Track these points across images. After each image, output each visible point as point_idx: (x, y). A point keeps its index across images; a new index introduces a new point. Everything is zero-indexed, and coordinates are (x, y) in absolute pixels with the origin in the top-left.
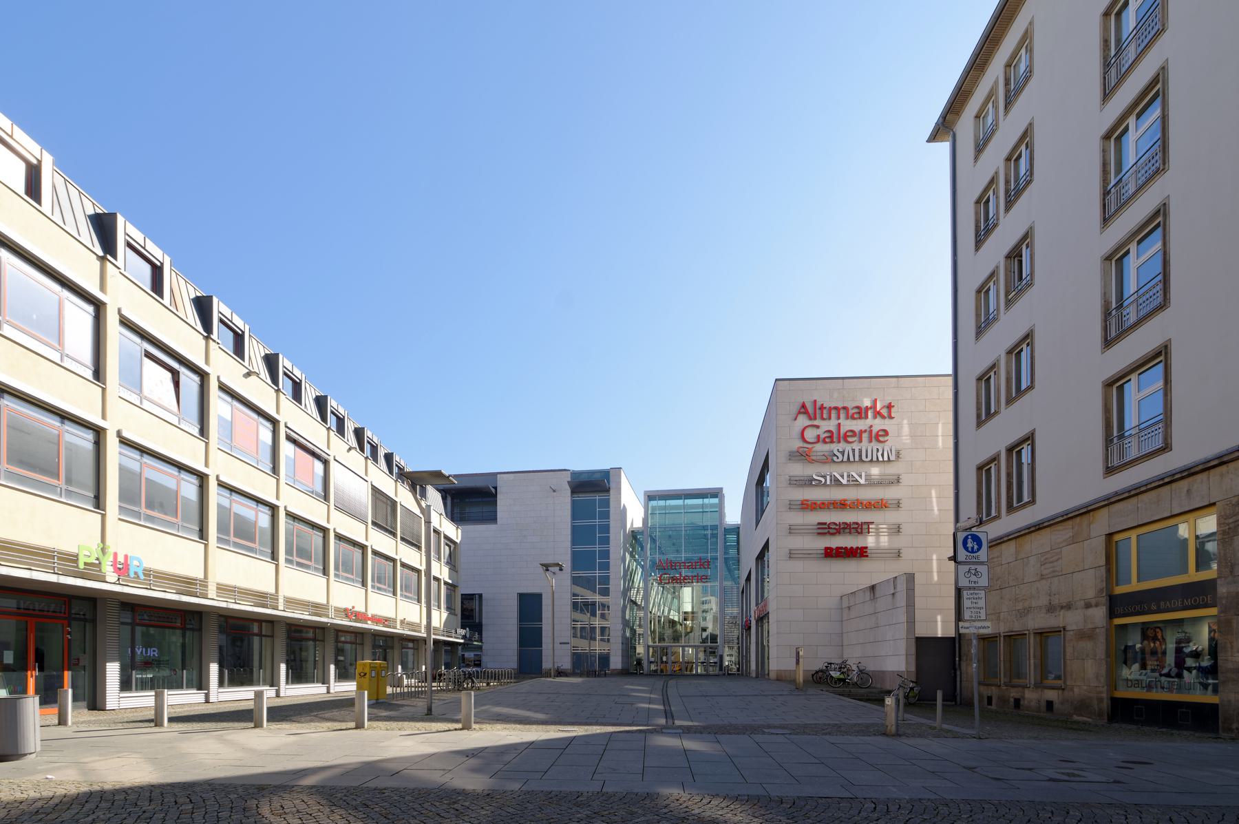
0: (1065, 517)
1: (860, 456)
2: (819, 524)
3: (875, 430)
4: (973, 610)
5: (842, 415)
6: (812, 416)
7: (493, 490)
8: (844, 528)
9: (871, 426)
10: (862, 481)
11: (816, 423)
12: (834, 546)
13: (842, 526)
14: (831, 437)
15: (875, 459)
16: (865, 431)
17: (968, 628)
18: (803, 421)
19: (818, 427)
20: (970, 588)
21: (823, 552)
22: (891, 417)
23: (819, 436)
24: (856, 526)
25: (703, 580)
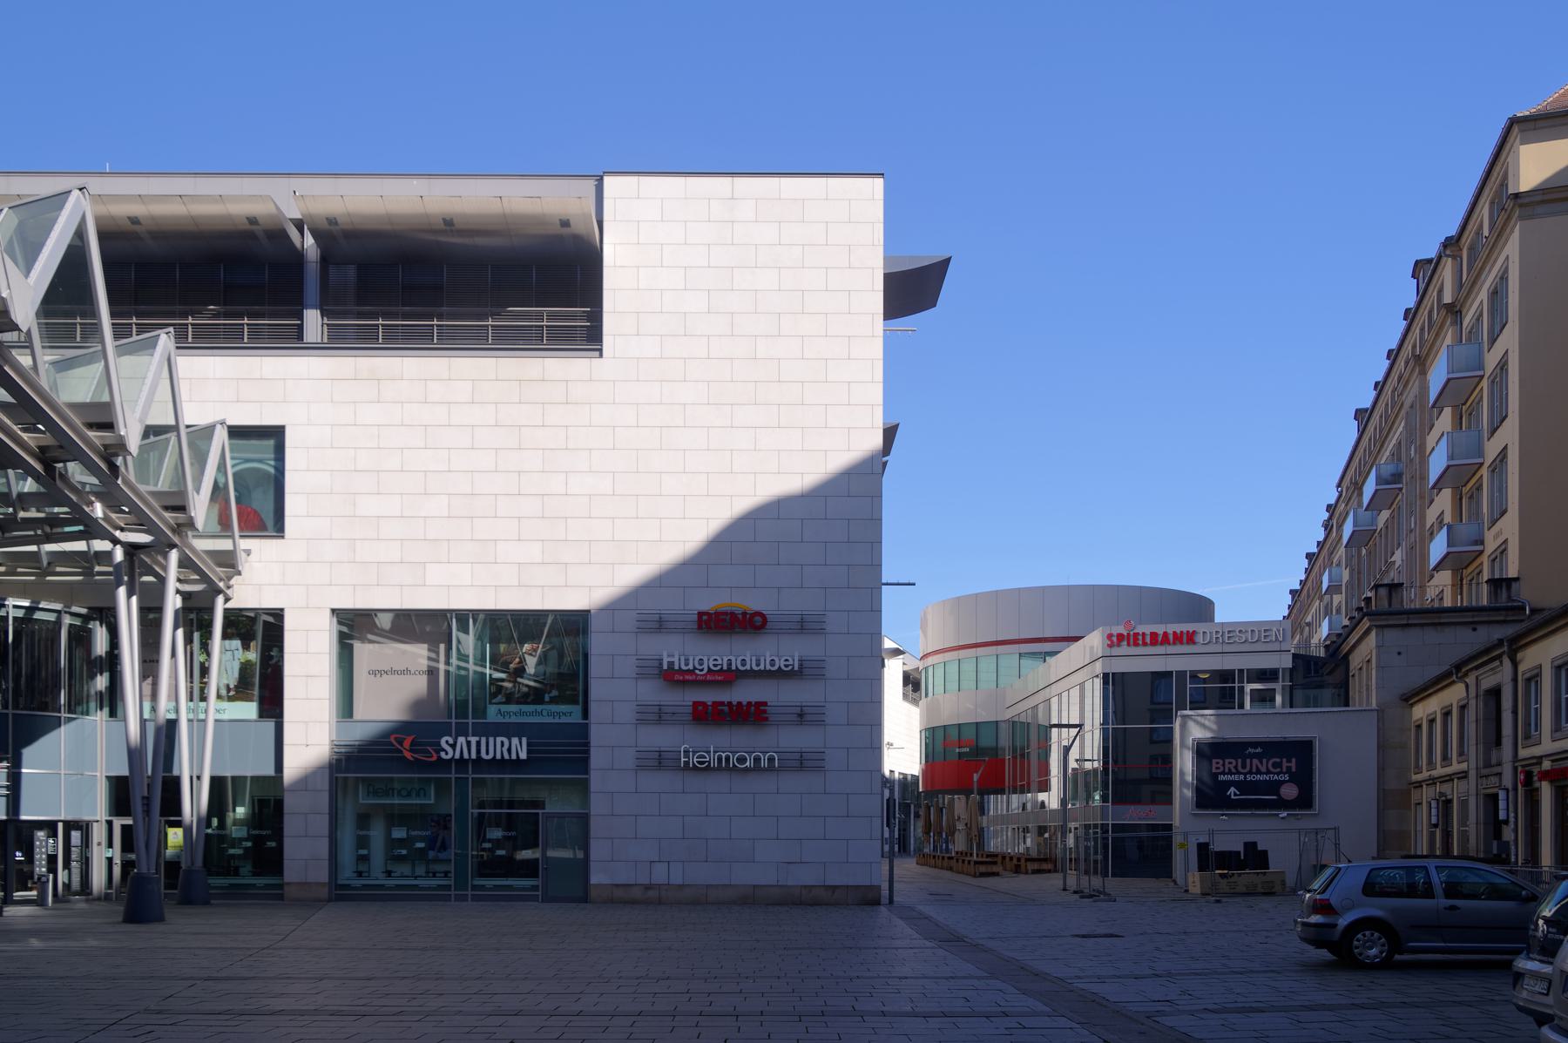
1: (478, 751)
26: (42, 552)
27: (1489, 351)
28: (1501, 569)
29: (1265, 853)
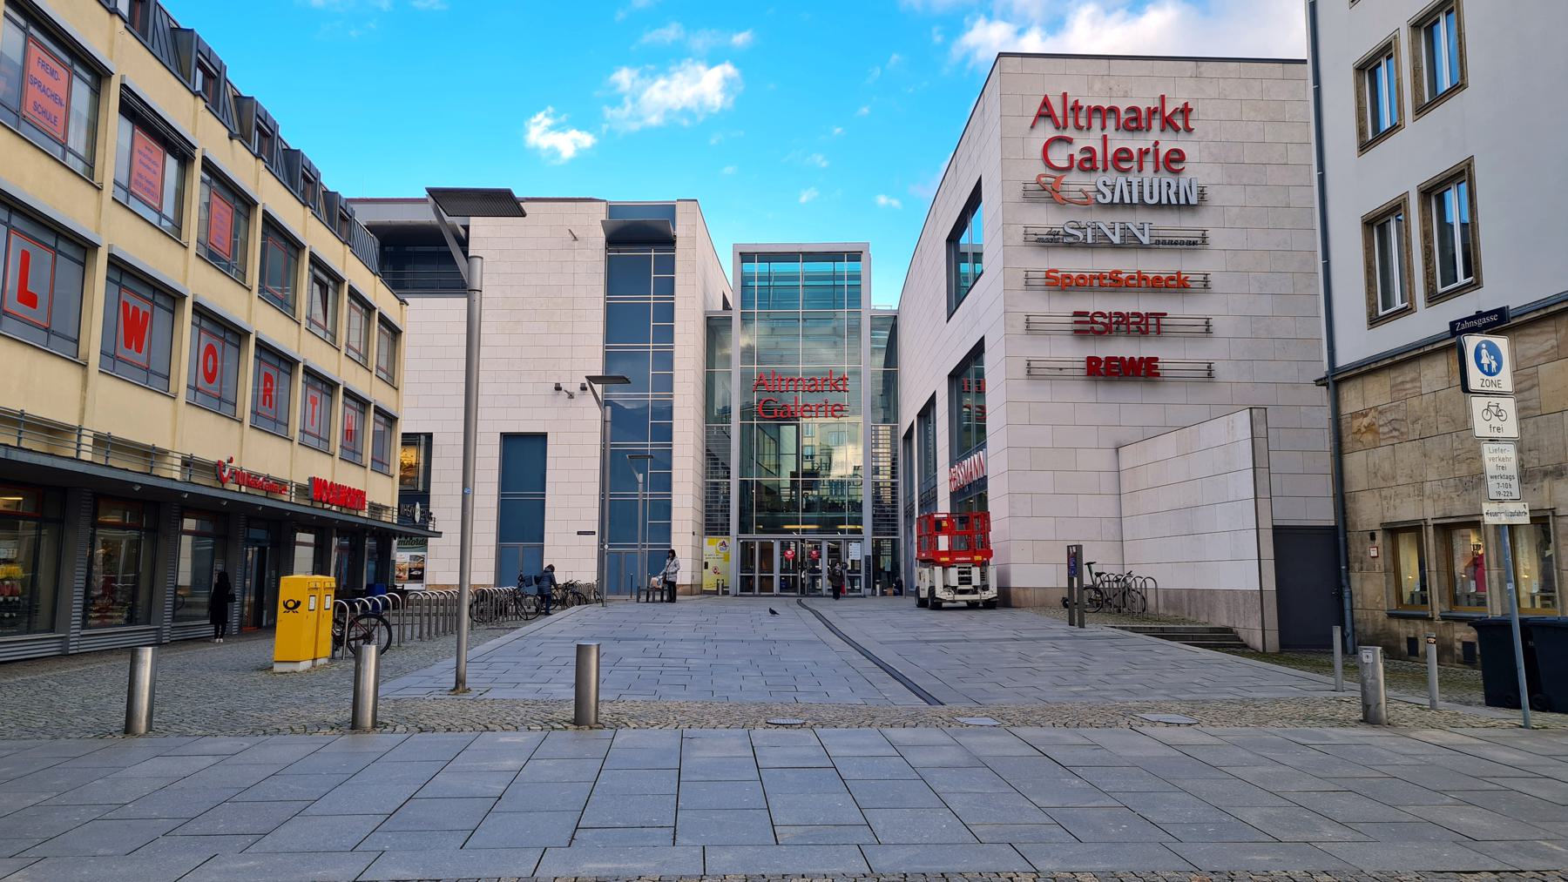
0: (1543, 312)
1: (1141, 193)
2: (1076, 314)
3: (1163, 151)
4: (1499, 480)
5: (1111, 123)
6: (1060, 120)
7: (462, 232)
8: (1116, 322)
9: (1157, 143)
10: (1146, 240)
11: (1067, 134)
12: (1102, 356)
13: (1114, 320)
14: (1092, 159)
15: (1164, 201)
16: (1147, 151)
17: (1496, 514)
18: (1047, 131)
19: (1069, 141)
20: (1492, 440)
21: (1084, 365)
22: (1189, 130)
23: (1071, 157)
24: (1138, 320)
25: (835, 413)
26: (1448, 604)
27: (913, 422)
28: (1562, 613)
29: (314, 481)
